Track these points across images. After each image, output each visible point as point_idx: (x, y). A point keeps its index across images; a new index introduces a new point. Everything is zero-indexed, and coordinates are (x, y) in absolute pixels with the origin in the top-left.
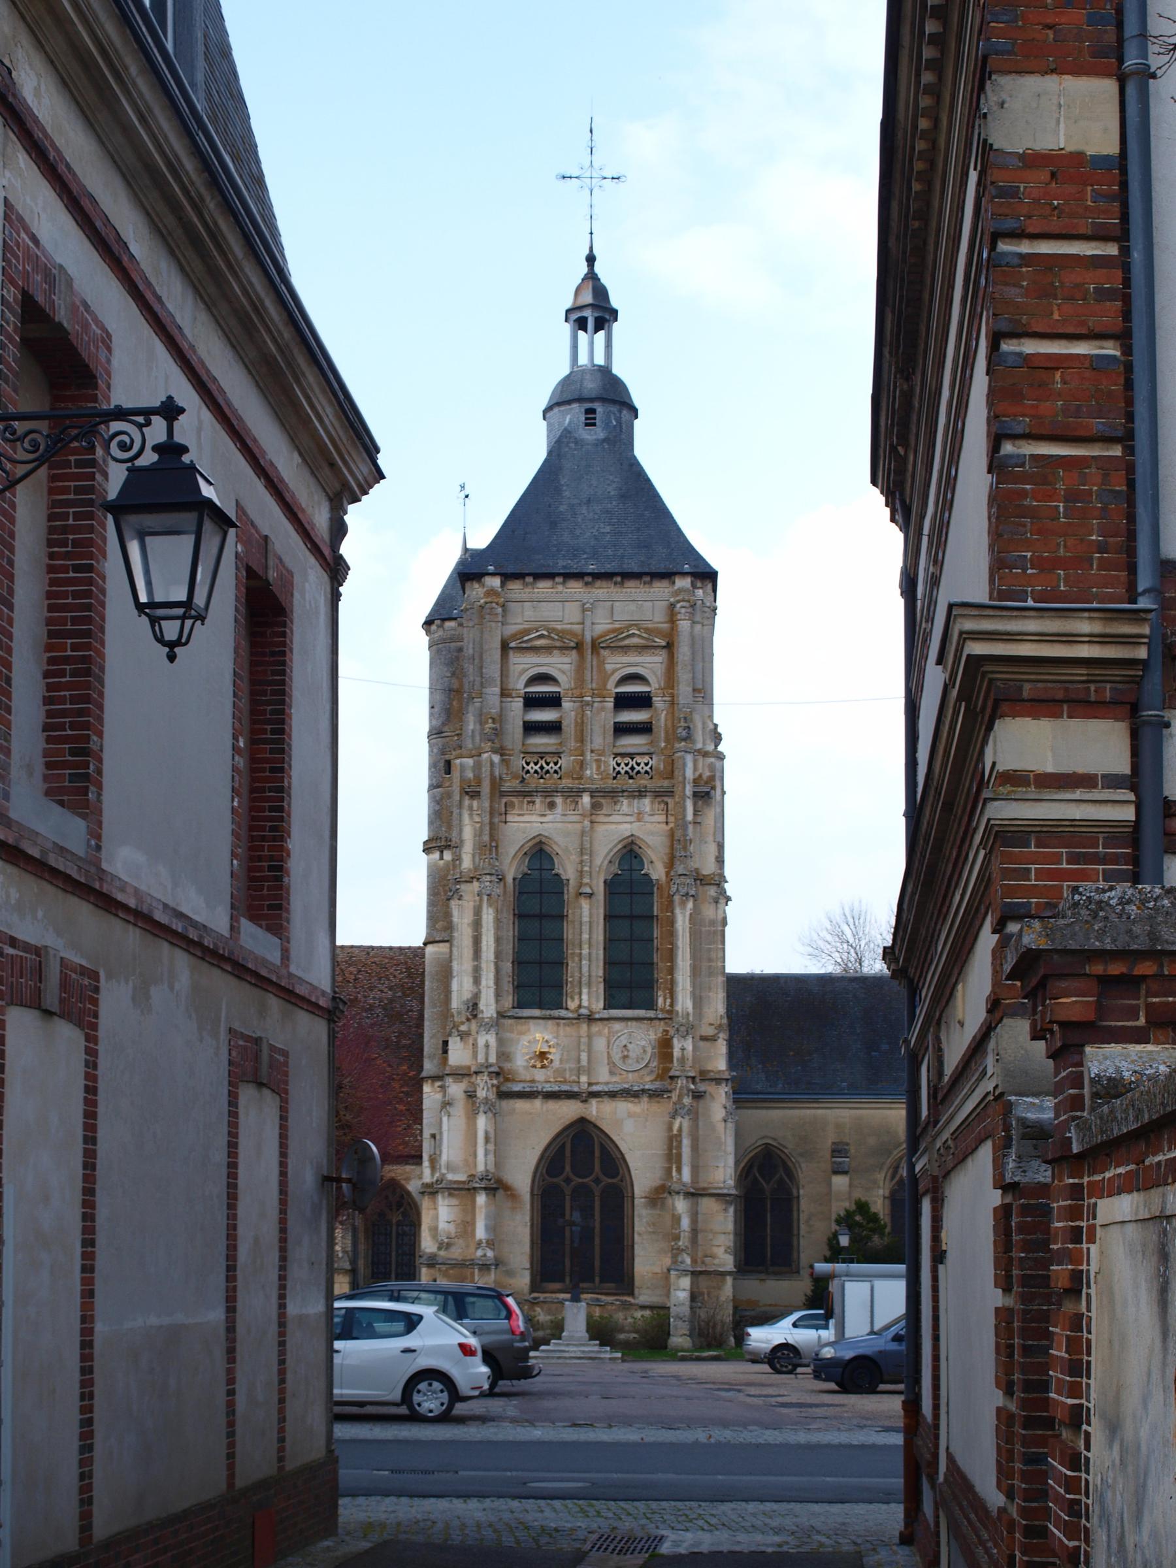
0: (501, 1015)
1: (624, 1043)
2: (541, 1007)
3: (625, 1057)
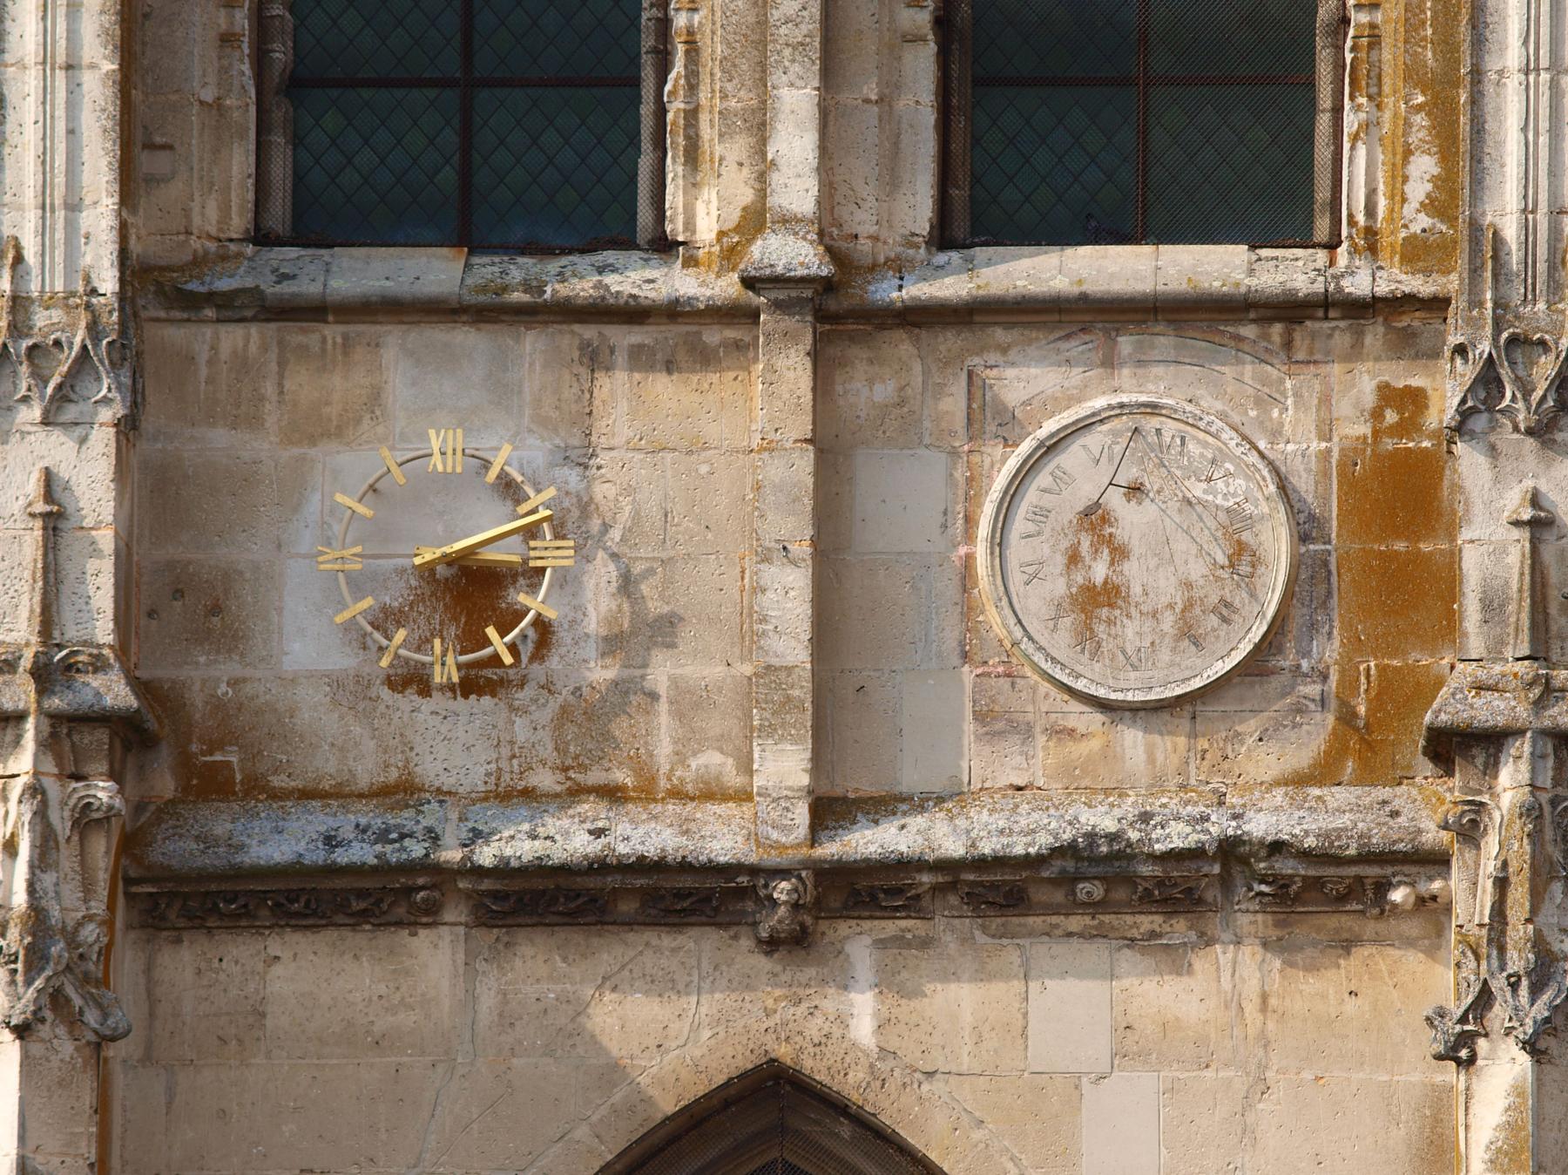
0: (157, 286)
1: (1085, 491)
2: (469, 237)
3: (1097, 601)
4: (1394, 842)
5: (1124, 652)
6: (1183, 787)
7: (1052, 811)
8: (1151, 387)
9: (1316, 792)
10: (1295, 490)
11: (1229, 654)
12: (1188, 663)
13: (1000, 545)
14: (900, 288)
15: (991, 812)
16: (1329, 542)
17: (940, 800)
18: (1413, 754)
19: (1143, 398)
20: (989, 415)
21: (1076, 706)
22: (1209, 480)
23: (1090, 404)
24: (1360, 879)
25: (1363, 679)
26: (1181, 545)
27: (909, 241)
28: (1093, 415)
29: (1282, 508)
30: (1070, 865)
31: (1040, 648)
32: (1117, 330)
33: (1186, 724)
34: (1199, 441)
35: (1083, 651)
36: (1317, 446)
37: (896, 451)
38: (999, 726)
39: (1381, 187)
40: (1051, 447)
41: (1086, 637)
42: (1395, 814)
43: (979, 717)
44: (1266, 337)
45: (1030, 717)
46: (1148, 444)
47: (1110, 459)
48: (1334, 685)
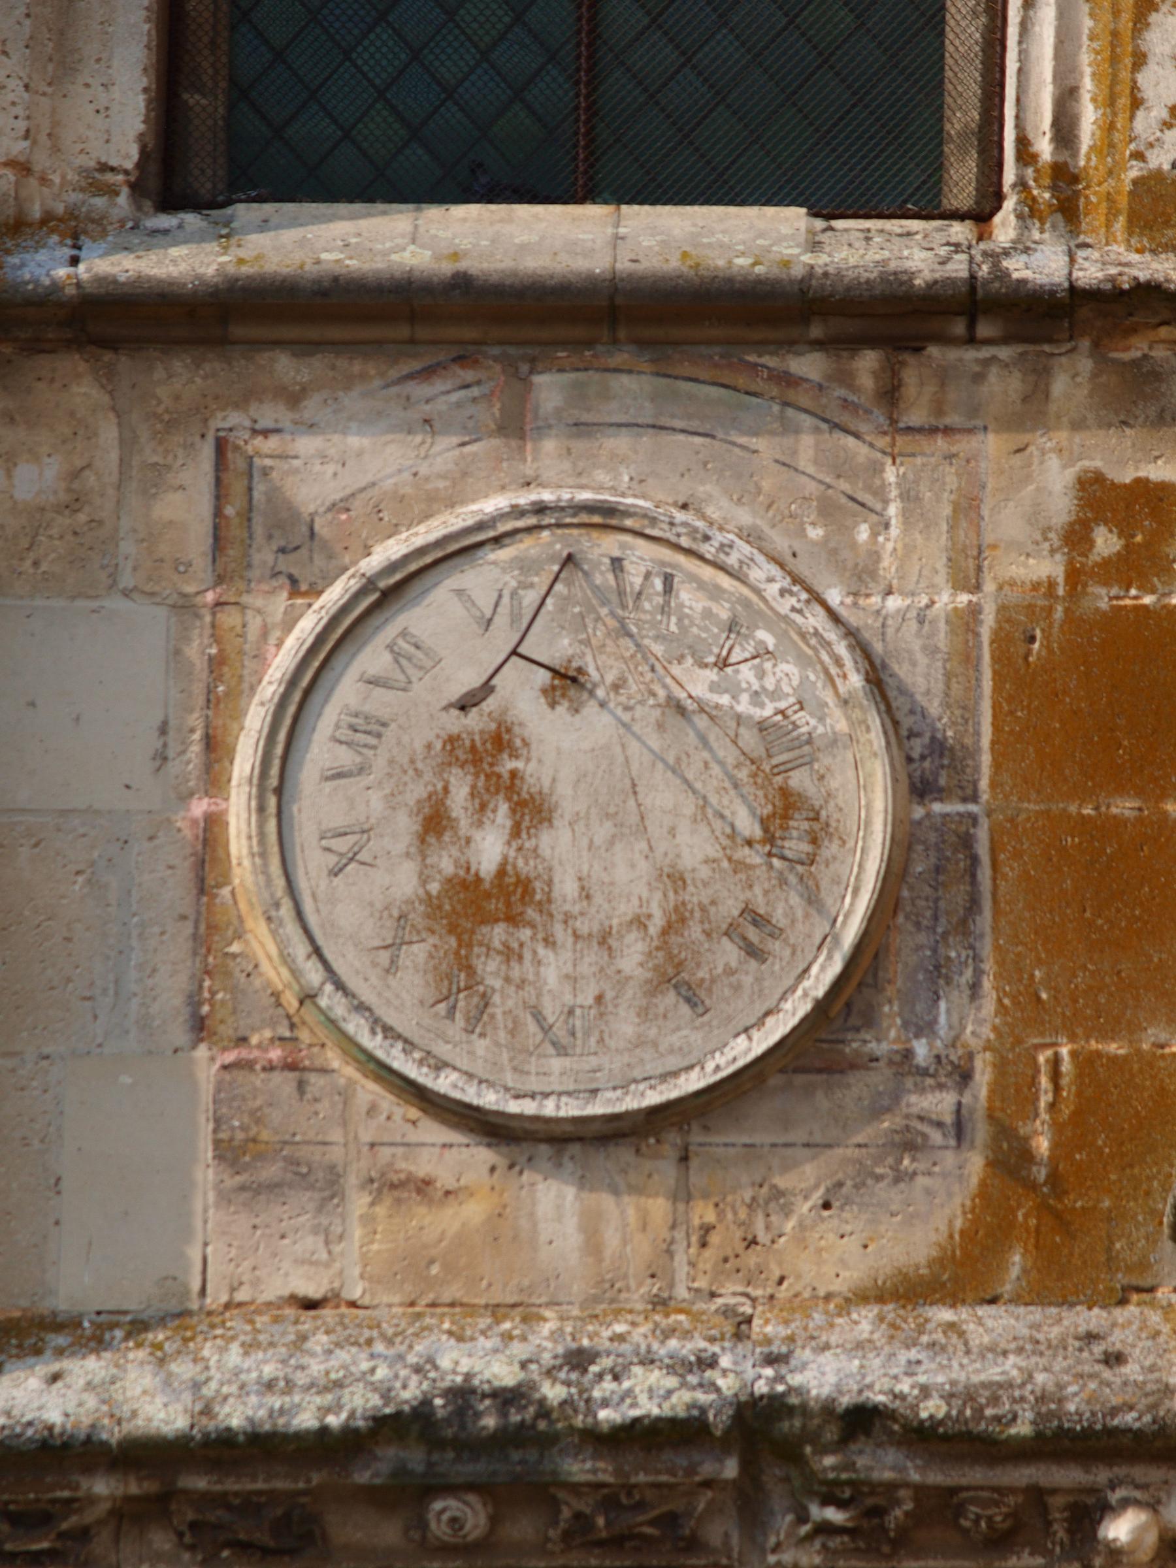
3: (480, 912)
4: (1114, 1411)
5: (538, 1016)
6: (660, 1303)
7: (379, 1347)
8: (601, 476)
9: (946, 1315)
10: (903, 691)
11: (760, 1022)
12: (675, 1039)
13: (279, 791)
14: (75, 261)
15: (248, 1348)
16: (974, 798)
17: (138, 1327)
18: (1152, 1240)
19: (585, 496)
20: (259, 530)
21: (433, 1132)
22: (723, 663)
23: (474, 507)
24: (1037, 1495)
25: (1044, 1082)
26: (662, 795)
27: (97, 179)
28: (480, 526)
29: (875, 722)
30: (415, 1458)
31: (362, 1008)
32: (533, 360)
33: (666, 1171)
34: (702, 585)
35: (451, 1013)
36: (948, 600)
37: (58, 603)
38: (271, 1171)
39: (1087, 84)
40: (390, 592)
41: (458, 988)
42: (1114, 1359)
43: (229, 1153)
44: (845, 378)
45: (336, 1154)
46: (596, 589)
47: (515, 618)
48: (984, 1093)
